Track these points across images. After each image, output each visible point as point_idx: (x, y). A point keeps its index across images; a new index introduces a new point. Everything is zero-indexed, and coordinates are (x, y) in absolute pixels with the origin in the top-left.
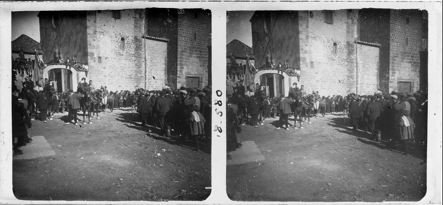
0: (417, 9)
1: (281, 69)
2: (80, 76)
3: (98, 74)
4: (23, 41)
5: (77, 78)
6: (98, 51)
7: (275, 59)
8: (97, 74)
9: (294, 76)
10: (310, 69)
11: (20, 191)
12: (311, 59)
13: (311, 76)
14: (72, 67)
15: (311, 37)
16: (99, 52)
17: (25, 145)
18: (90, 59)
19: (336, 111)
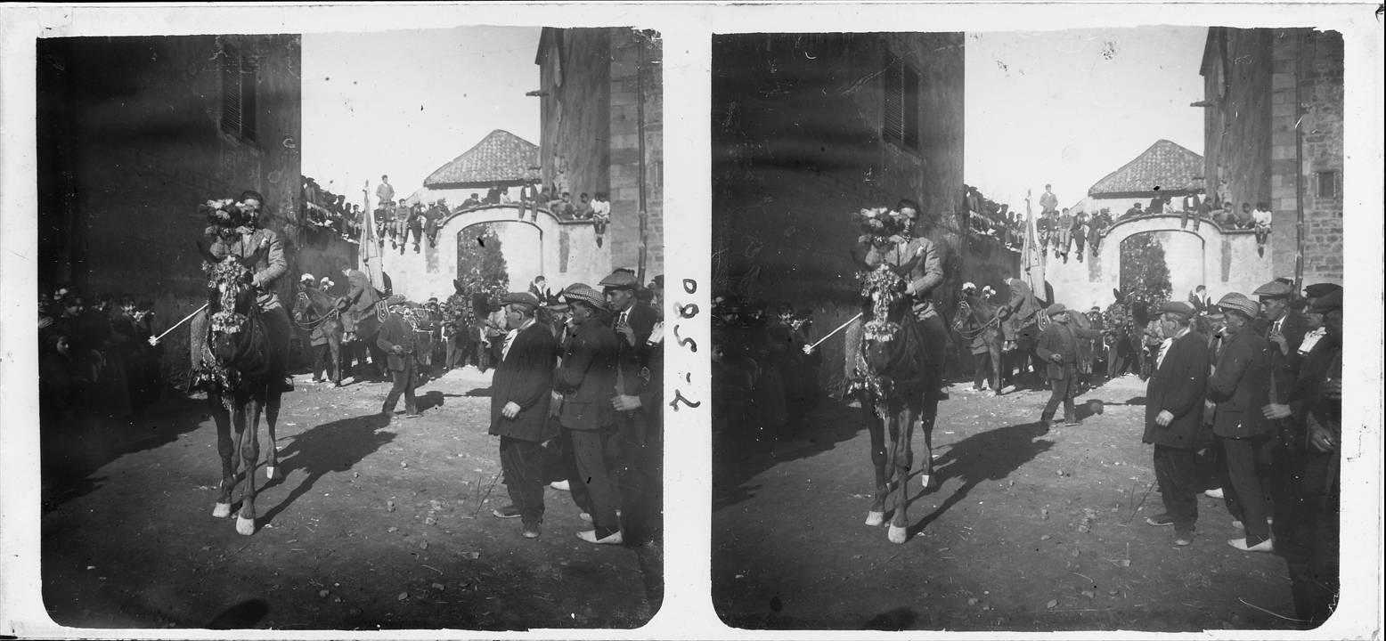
0: (629, 28)
1: (529, 202)
2: (575, 242)
3: (1315, 242)
4: (489, 151)
5: (1223, 258)
6: (1318, 152)
7: (568, 170)
8: (1311, 240)
9: (582, 223)
10: (1317, 203)
11: (65, 596)
12: (1324, 163)
13: (1321, 226)
14: (539, 213)
15: (1325, 74)
16: (1324, 153)
17: (175, 439)
18: (1283, 186)
19: (1338, 391)
